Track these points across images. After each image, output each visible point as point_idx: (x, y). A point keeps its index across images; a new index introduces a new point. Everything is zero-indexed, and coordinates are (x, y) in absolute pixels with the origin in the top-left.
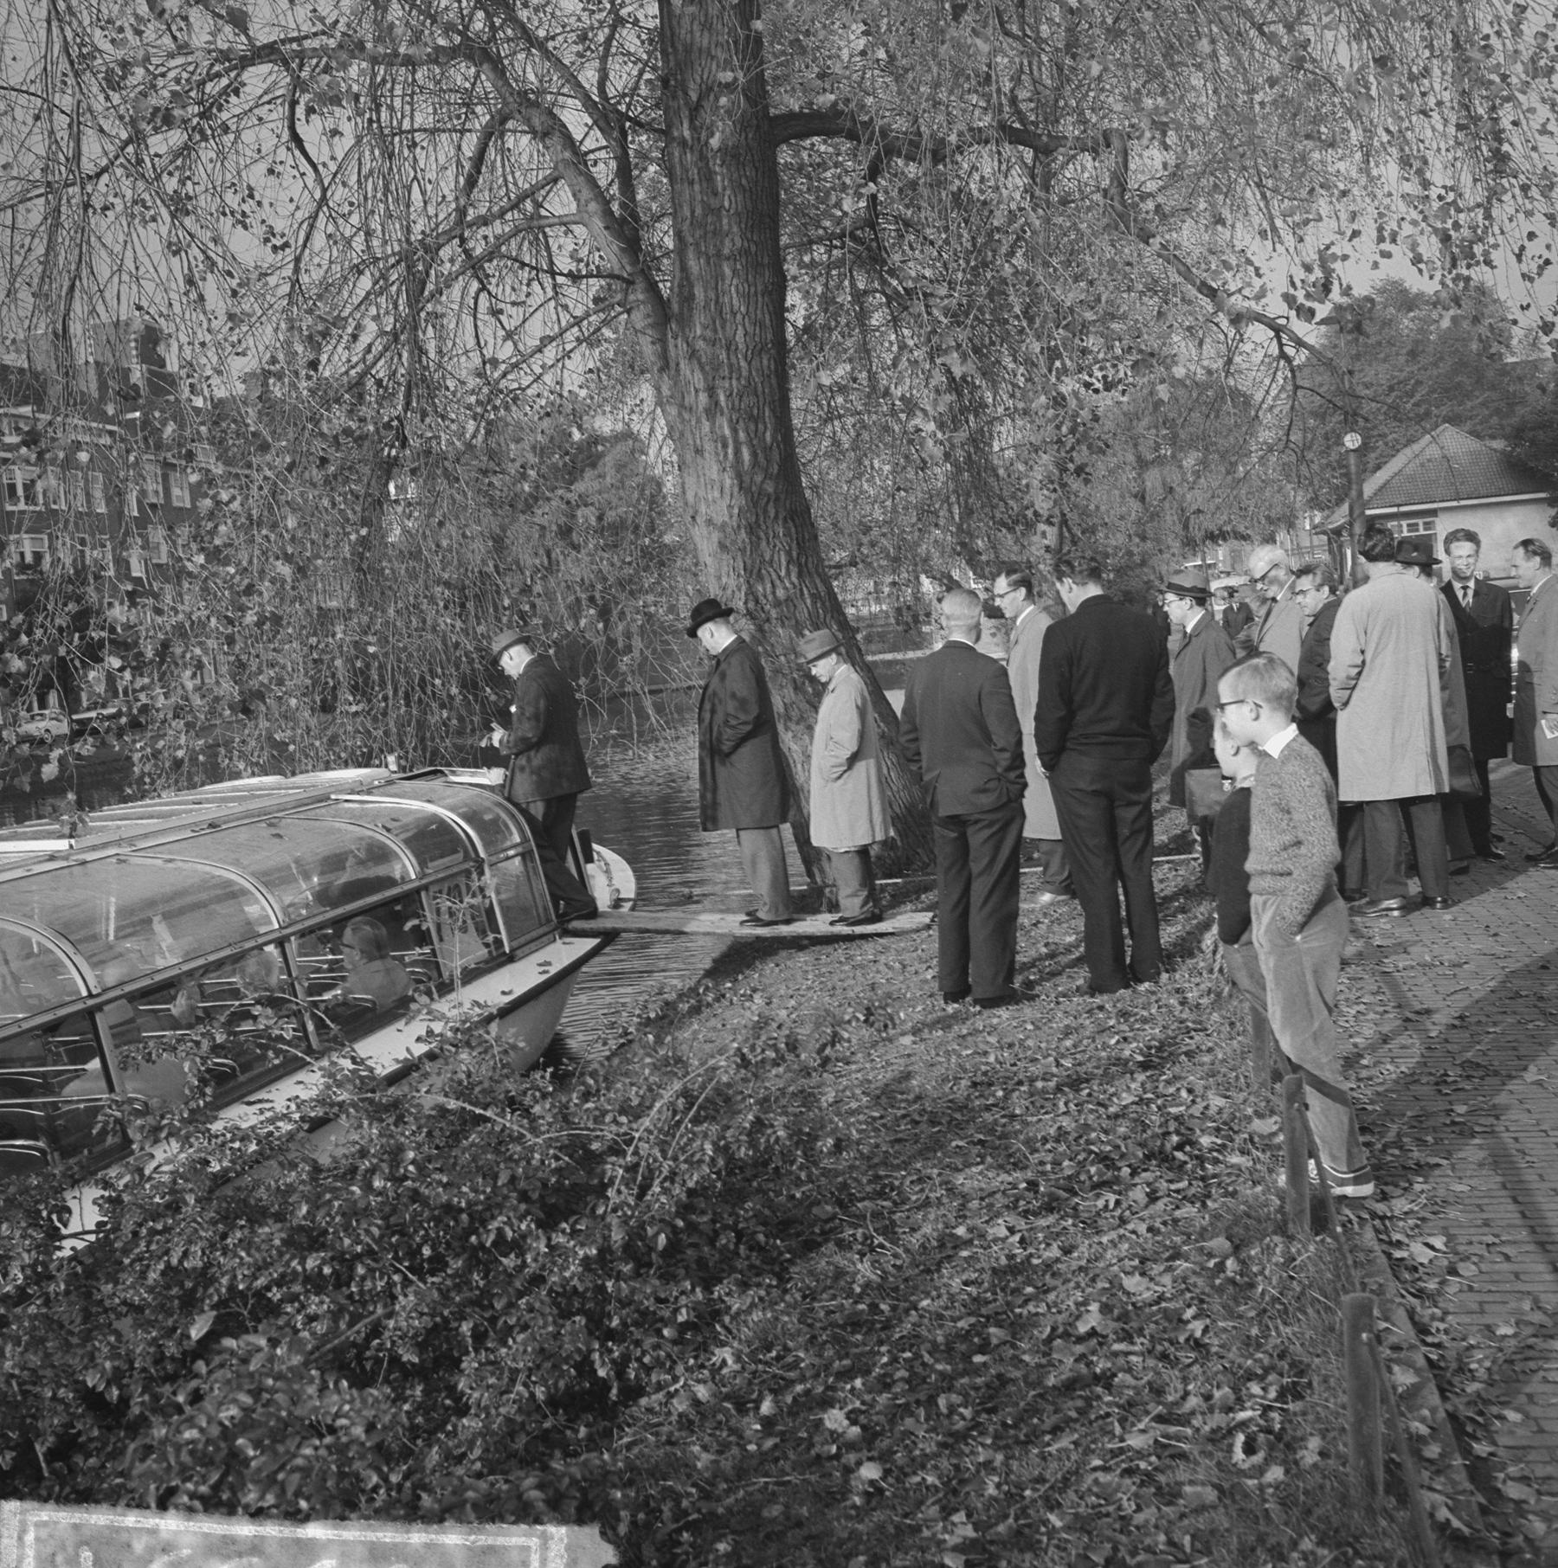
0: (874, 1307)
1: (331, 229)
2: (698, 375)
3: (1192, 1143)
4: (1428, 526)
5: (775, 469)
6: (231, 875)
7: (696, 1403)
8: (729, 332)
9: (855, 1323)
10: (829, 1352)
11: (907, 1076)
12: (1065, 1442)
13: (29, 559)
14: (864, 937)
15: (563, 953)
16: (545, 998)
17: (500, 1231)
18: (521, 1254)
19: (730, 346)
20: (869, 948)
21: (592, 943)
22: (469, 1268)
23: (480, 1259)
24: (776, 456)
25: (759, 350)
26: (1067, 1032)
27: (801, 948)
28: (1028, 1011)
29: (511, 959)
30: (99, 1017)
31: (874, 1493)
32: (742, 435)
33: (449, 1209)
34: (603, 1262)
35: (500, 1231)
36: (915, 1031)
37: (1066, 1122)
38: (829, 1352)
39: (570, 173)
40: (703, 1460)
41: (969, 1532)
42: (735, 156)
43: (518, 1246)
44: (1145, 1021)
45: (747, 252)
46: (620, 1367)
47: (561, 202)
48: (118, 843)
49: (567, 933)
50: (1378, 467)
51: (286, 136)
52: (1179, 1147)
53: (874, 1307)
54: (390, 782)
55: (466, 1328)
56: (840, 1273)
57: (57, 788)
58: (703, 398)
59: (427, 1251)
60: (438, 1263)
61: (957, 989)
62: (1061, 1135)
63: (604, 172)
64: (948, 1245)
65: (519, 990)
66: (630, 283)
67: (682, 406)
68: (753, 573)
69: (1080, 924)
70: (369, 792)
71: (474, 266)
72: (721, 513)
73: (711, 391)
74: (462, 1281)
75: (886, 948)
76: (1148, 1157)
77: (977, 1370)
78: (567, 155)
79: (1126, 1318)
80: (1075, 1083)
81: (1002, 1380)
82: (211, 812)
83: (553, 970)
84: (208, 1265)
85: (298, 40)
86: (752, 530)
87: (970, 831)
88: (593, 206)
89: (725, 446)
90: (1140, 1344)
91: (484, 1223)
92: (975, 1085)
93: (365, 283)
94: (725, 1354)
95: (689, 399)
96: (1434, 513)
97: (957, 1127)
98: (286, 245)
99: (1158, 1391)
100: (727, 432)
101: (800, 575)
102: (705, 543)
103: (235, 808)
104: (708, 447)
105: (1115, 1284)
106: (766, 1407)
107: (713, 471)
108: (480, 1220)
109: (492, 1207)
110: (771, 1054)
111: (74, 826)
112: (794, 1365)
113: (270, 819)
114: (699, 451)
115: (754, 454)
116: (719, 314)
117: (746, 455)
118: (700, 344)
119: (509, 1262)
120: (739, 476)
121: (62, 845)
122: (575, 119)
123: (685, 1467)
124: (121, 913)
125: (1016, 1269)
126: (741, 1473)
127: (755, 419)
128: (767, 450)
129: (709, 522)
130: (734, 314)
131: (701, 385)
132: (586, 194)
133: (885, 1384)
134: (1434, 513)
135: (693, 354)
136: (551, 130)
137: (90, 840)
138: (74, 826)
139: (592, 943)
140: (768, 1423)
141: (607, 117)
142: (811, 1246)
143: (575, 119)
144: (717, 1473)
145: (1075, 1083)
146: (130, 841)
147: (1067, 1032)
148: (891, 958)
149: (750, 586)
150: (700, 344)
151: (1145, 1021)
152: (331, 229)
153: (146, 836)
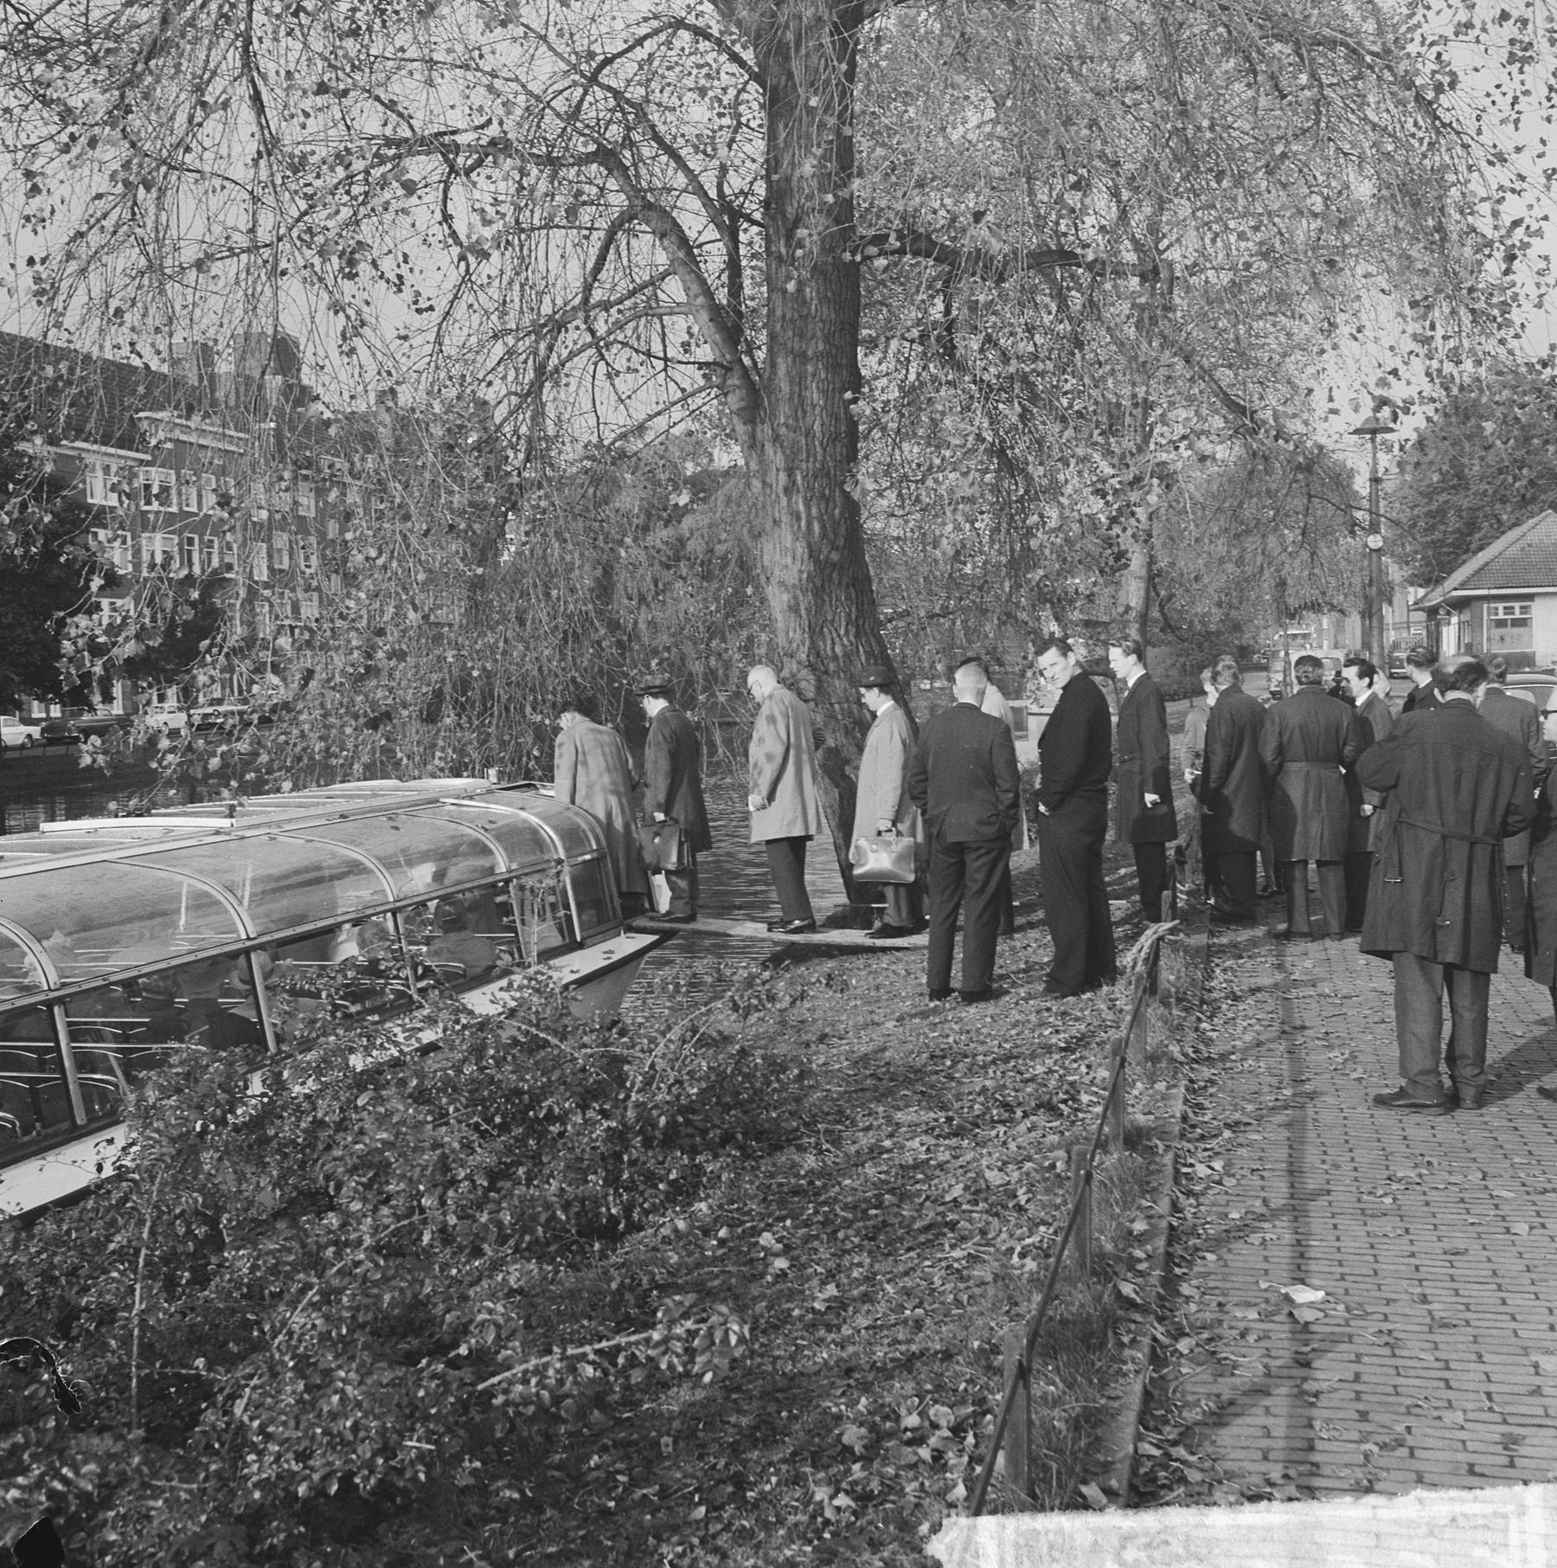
0: (811, 1183)
1: (471, 300)
2: (779, 456)
3: (1075, 1100)
4: (1524, 609)
5: (841, 542)
6: (355, 854)
7: (676, 1231)
8: (809, 420)
9: (797, 1191)
10: (773, 1207)
11: (884, 1049)
12: (912, 1254)
13: (159, 559)
14: (884, 950)
15: (625, 944)
16: (608, 981)
17: (550, 1109)
18: (564, 1124)
19: (808, 433)
20: (885, 960)
21: (652, 938)
22: (526, 1135)
23: (537, 1129)
24: (842, 530)
25: (834, 439)
26: (1015, 1025)
27: (831, 957)
28: (990, 1008)
29: (581, 946)
30: (253, 956)
31: (782, 1275)
32: (814, 511)
33: (518, 1092)
34: (619, 1137)
35: (550, 1109)
36: (900, 1019)
37: (988, 1083)
38: (773, 1207)
39: (681, 270)
40: (674, 1258)
41: (835, 1292)
42: (824, 273)
43: (563, 1119)
44: (1077, 1019)
45: (829, 354)
46: (628, 1209)
47: (674, 289)
48: (268, 824)
49: (630, 929)
50: (1481, 548)
51: (438, 216)
52: (1065, 1102)
53: (811, 1183)
54: (490, 792)
55: (521, 1171)
56: (794, 1165)
57: (223, 775)
58: (783, 476)
59: (498, 1120)
60: (504, 1128)
61: (940, 990)
62: (984, 1090)
63: (714, 260)
64: (875, 1152)
65: (585, 971)
66: (728, 369)
67: (764, 482)
68: (815, 632)
69: (1051, 949)
70: (471, 798)
71: (600, 345)
72: (791, 577)
73: (790, 472)
74: (521, 1141)
75: (899, 960)
76: (1038, 1107)
77: (869, 1218)
78: (681, 254)
79: (978, 1192)
80: (1007, 1058)
81: (885, 1224)
82: (343, 805)
83: (615, 957)
84: (344, 1119)
85: (453, 133)
86: (818, 592)
87: (969, 858)
88: (701, 300)
89: (799, 519)
90: (982, 1206)
91: (539, 1102)
92: (932, 1057)
93: (499, 350)
94: (703, 1206)
95: (771, 478)
96: (1531, 597)
97: (908, 1083)
98: (431, 308)
99: (983, 1232)
100: (801, 508)
101: (857, 635)
102: (778, 600)
103: (360, 804)
104: (785, 519)
105: (980, 1174)
106: (723, 1233)
107: (788, 539)
108: (536, 1101)
109: (546, 1091)
110: (755, 1002)
111: (232, 808)
112: (748, 1213)
113: (391, 815)
114: (776, 523)
115: (823, 528)
116: (800, 404)
117: (816, 527)
118: (783, 430)
119: (555, 1129)
120: (809, 545)
121: (225, 823)
122: (693, 219)
123: (664, 1263)
124: (254, 882)
125: (918, 1165)
126: (698, 1265)
127: (827, 500)
128: (836, 524)
129: (782, 583)
130: (814, 407)
131: (782, 465)
132: (695, 288)
133: (806, 1224)
134: (1531, 597)
135: (776, 438)
136: (670, 231)
137: (246, 821)
138: (232, 808)
139: (652, 938)
140: (722, 1242)
141: (728, 216)
142: (777, 1147)
143: (693, 219)
144: (680, 1265)
145: (1007, 1058)
146: (279, 824)
147: (1015, 1025)
148: (900, 969)
149: (813, 642)
150: (783, 430)
151: (1077, 1019)
152: (471, 300)
153: (290, 821)
